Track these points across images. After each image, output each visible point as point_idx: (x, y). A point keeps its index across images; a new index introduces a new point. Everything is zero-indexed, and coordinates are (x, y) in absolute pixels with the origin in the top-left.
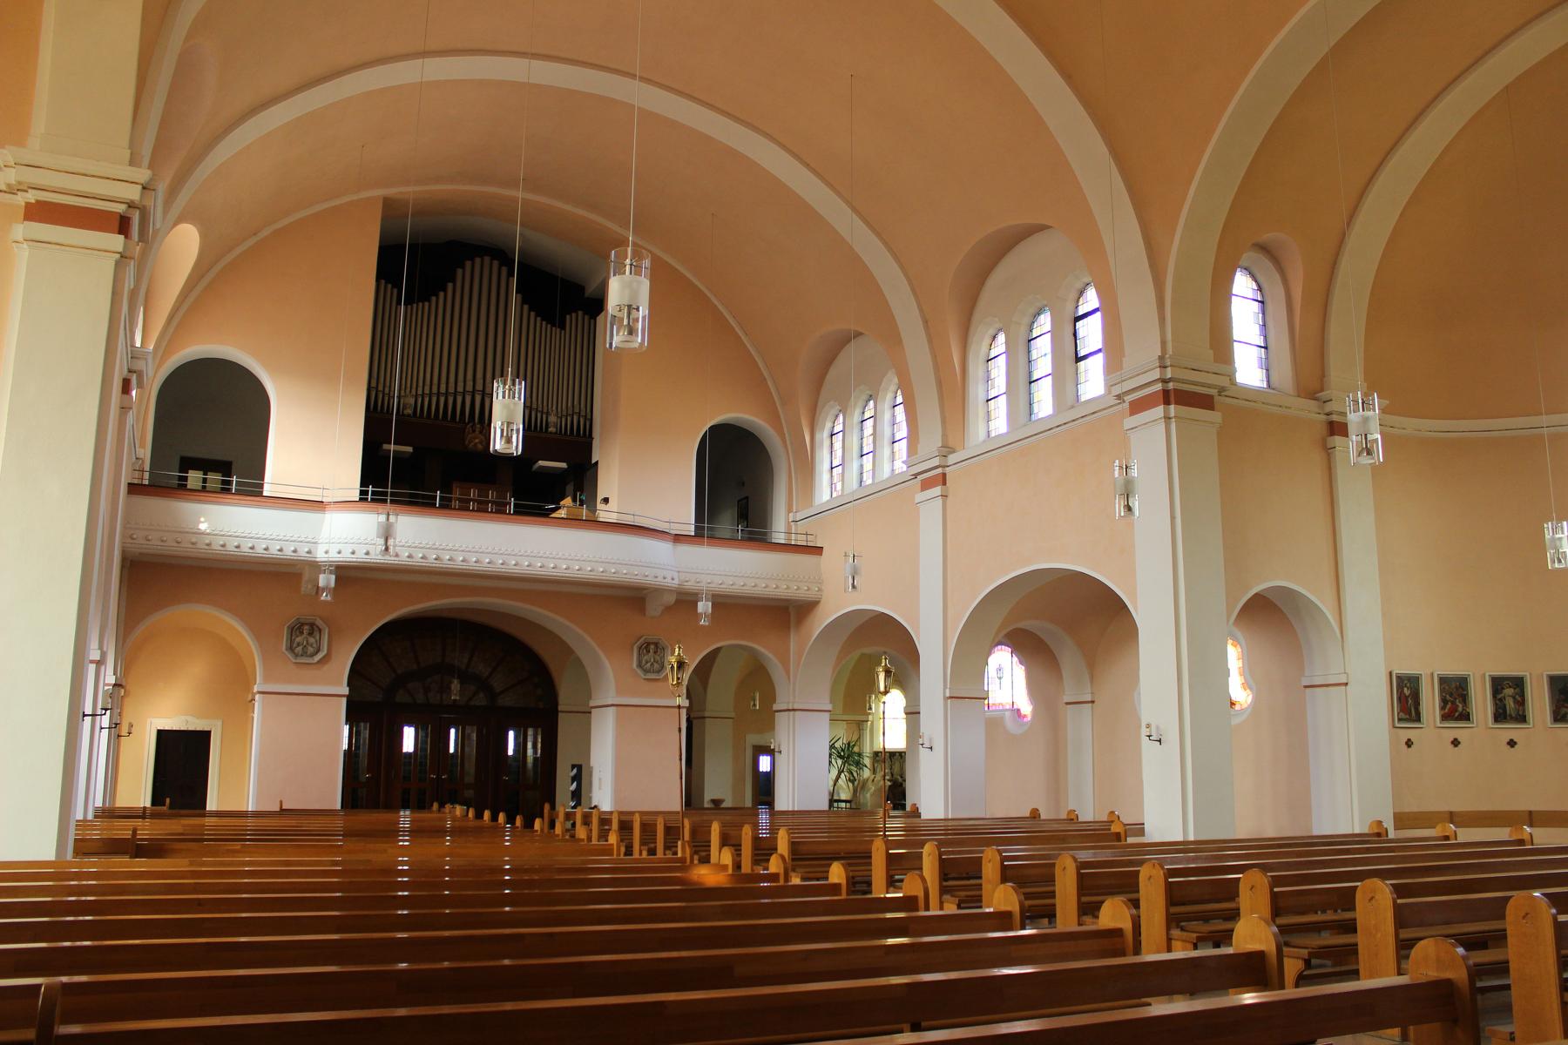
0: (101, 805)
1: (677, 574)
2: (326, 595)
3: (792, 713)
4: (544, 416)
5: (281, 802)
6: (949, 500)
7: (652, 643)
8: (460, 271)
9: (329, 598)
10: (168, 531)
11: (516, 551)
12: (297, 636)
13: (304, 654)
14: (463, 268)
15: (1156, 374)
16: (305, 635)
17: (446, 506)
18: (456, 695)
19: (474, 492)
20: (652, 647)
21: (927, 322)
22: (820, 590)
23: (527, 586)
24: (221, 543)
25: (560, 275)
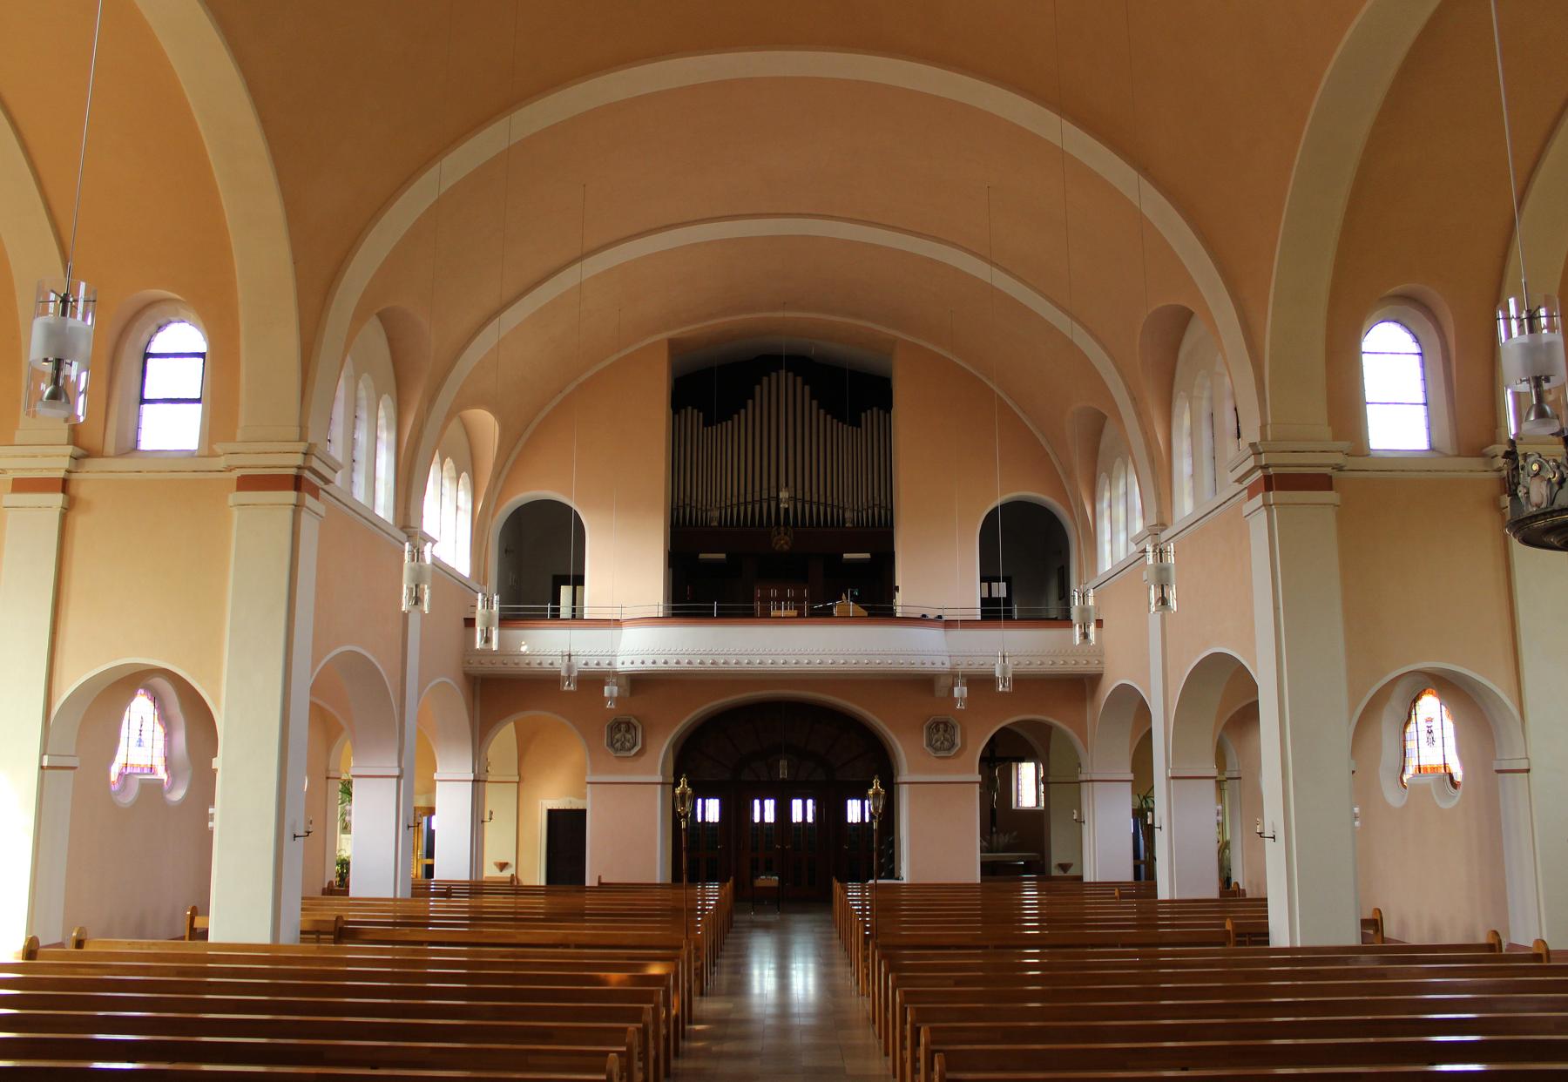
0: (468, 879)
1: (948, 658)
3: (1090, 784)
4: (841, 511)
5: (600, 877)
7: (941, 723)
8: (758, 388)
9: (613, 706)
13: (623, 748)
14: (760, 383)
15: (1250, 463)
20: (942, 726)
22: (1100, 662)
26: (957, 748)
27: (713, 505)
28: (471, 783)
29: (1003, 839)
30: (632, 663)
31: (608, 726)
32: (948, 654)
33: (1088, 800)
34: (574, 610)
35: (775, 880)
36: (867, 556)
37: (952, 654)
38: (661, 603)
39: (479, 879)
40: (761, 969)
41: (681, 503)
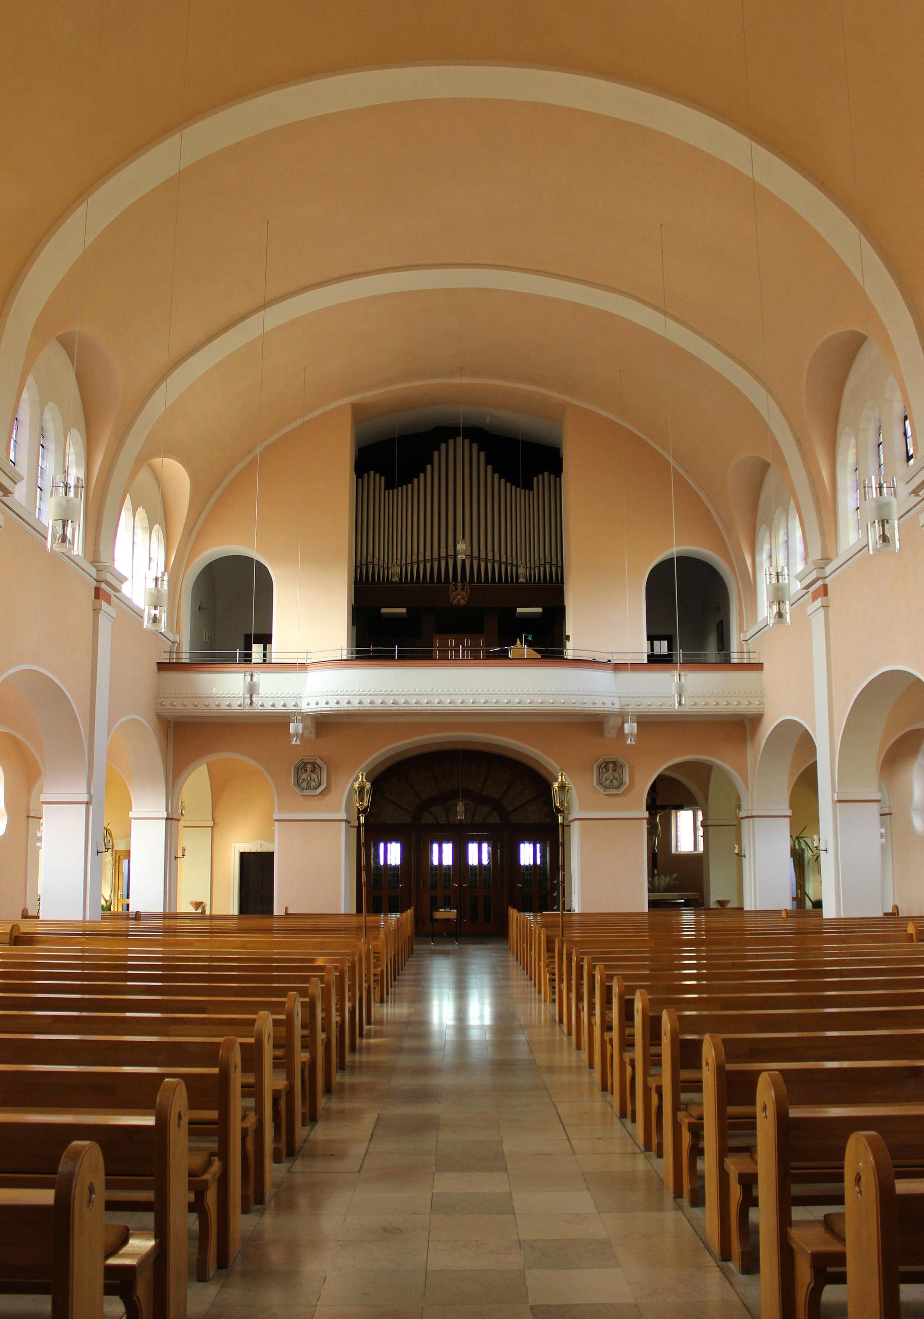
1: (618, 699)
2: (296, 740)
4: (514, 568)
5: (286, 909)
6: (830, 611)
8: (436, 454)
9: (298, 742)
10: (187, 697)
11: (463, 691)
12: (303, 774)
13: (309, 788)
14: (439, 450)
16: (308, 773)
17: (444, 658)
18: (461, 815)
19: (452, 642)
20: (611, 765)
21: (799, 440)
22: (761, 703)
23: (502, 719)
24: (227, 703)
25: (520, 439)
26: (626, 786)
27: (394, 563)
28: (165, 820)
29: (664, 881)
30: (317, 704)
31: (294, 767)
32: (618, 695)
33: (749, 830)
34: (265, 655)
35: (454, 912)
36: (539, 610)
37: (621, 695)
38: (345, 647)
39: (173, 911)
40: (441, 1000)
41: (364, 562)
